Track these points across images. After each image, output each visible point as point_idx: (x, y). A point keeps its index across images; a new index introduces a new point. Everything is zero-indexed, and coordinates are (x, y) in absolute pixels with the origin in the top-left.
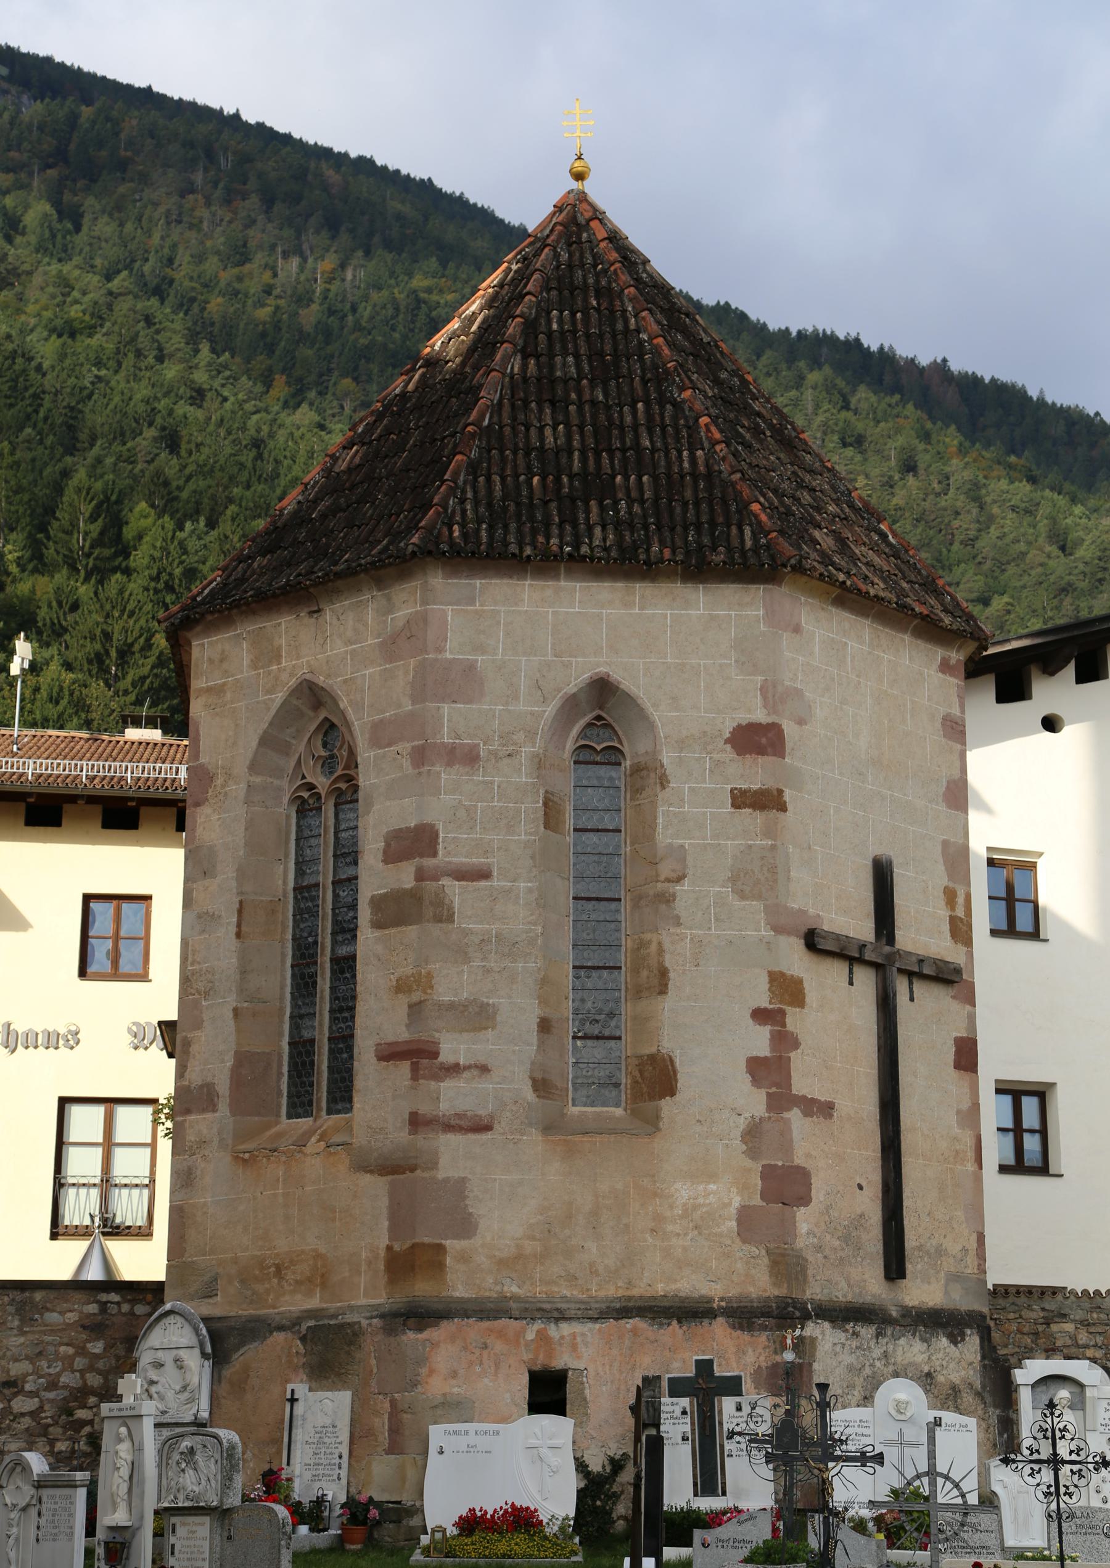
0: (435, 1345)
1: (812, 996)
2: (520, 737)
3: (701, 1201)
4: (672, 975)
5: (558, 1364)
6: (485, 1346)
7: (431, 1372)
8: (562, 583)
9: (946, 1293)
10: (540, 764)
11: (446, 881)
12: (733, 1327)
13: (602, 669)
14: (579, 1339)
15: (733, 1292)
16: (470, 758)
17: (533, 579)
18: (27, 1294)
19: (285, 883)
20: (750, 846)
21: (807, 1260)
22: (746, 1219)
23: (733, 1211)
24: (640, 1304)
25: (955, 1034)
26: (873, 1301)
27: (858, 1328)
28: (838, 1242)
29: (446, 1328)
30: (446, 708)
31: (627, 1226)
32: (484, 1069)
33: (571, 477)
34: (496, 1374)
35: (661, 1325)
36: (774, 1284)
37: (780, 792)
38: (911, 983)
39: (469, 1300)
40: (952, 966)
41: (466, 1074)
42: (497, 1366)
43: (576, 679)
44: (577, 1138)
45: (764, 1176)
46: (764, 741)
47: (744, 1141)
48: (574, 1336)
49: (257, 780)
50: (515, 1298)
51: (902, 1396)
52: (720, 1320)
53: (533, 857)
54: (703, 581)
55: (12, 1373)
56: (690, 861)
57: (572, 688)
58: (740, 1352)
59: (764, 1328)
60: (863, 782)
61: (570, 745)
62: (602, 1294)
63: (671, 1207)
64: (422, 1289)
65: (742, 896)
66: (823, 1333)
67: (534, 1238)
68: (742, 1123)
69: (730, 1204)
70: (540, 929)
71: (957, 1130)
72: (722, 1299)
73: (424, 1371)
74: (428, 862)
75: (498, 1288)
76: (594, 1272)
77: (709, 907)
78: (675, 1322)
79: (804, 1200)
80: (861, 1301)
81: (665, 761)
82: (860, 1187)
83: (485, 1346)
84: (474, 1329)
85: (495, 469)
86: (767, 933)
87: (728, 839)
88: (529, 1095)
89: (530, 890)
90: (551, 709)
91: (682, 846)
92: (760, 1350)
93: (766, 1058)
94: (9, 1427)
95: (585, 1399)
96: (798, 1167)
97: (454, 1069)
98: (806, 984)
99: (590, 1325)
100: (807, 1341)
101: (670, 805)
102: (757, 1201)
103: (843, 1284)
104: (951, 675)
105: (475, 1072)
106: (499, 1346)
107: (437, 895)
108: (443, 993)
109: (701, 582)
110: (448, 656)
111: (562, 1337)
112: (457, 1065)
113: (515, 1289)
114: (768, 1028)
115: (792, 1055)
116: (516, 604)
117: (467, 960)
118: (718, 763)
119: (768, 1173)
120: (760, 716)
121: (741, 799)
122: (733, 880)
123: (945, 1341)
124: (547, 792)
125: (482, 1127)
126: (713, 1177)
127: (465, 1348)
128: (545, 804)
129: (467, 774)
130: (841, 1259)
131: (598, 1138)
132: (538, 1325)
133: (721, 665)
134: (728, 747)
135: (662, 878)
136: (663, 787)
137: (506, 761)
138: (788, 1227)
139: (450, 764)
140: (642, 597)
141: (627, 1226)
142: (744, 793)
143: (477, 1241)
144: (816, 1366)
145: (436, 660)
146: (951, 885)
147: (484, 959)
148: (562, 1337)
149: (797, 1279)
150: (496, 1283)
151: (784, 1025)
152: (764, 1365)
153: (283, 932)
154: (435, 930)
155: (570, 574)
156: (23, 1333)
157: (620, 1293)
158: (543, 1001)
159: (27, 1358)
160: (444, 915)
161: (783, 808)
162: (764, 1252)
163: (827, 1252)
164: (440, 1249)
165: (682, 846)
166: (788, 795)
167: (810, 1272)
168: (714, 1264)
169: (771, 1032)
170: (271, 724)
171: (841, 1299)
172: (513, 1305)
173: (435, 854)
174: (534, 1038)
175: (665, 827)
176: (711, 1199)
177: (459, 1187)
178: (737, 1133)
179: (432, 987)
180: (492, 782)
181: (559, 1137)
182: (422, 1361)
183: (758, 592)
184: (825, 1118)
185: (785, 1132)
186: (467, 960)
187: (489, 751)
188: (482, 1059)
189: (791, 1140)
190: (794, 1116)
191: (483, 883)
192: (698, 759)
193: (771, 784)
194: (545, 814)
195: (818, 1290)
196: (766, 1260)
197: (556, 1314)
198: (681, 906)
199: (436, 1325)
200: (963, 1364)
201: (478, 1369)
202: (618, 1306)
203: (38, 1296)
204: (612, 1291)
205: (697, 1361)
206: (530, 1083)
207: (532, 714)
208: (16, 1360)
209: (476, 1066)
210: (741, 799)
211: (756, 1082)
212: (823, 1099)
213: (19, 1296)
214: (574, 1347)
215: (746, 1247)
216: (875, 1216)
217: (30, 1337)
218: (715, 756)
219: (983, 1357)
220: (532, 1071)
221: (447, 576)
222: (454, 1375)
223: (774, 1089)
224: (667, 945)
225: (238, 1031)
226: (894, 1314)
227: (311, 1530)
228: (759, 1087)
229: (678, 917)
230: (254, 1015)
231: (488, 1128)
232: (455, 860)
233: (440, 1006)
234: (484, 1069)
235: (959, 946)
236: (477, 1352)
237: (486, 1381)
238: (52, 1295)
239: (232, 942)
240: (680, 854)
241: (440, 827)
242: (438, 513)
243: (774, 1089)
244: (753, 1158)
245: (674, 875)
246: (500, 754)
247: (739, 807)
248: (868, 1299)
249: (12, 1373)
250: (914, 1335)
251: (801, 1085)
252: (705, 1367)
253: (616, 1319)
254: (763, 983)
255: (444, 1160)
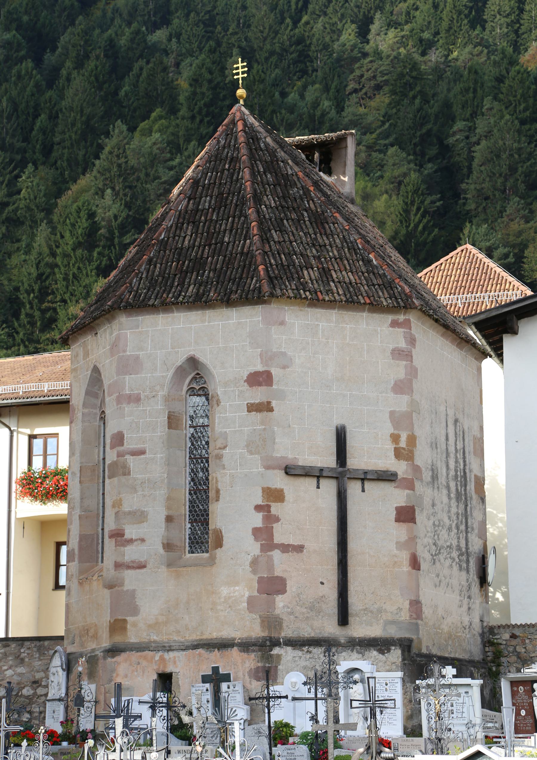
0: (119, 663)
1: (289, 495)
2: (158, 388)
3: (232, 595)
4: (221, 492)
5: (168, 670)
6: (139, 663)
7: (117, 675)
8: (175, 314)
9: (384, 629)
10: (167, 399)
11: (127, 457)
12: (241, 651)
13: (192, 353)
14: (177, 659)
15: (245, 635)
16: (136, 399)
17: (163, 314)
18: (42, 643)
19: (99, 456)
20: (255, 430)
21: (282, 619)
22: (251, 601)
23: (245, 598)
24: (205, 642)
25: (395, 505)
26: (330, 636)
27: (310, 649)
28: (305, 610)
29: (124, 655)
30: (127, 377)
31: (201, 607)
32: (143, 540)
33: (190, 261)
34: (143, 676)
35: (211, 651)
36: (262, 631)
37: (269, 403)
38: (363, 484)
39: (136, 643)
40: (390, 473)
41: (135, 543)
42: (143, 672)
43: (181, 359)
44: (181, 569)
45: (259, 582)
46: (261, 379)
47: (251, 567)
48: (175, 657)
49: (86, 411)
50: (155, 642)
51: (294, 680)
52: (235, 648)
53: (163, 443)
54: (235, 306)
55: (37, 677)
56: (229, 438)
57: (179, 363)
58: (243, 662)
59: (254, 651)
60: (330, 390)
61: (185, 388)
62: (191, 638)
63: (219, 598)
64: (118, 639)
65: (251, 453)
66: (286, 652)
67: (162, 615)
68: (250, 558)
69: (244, 595)
70: (166, 475)
71: (395, 552)
72: (239, 639)
73: (114, 675)
74: (121, 449)
75: (148, 638)
76: (187, 629)
77: (237, 459)
78: (216, 650)
79: (283, 591)
80: (321, 636)
81: (219, 393)
82: (322, 583)
83: (139, 663)
84: (134, 656)
85: (159, 261)
86: (261, 469)
87: (246, 427)
88: (161, 551)
89: (162, 458)
90: (170, 374)
91: (226, 432)
92: (251, 661)
93: (260, 528)
94: (36, 701)
95: (179, 685)
96: (277, 577)
97: (131, 541)
98: (285, 491)
99: (181, 652)
100: (275, 657)
101: (221, 413)
102: (256, 593)
103: (310, 630)
104: (398, 328)
105: (139, 542)
106: (144, 663)
107: (124, 463)
108: (126, 508)
109: (234, 307)
110: (128, 353)
111: (170, 658)
112: (132, 539)
113: (155, 638)
114: (262, 513)
115: (275, 525)
116: (156, 327)
117: (136, 491)
118: (241, 392)
119: (261, 581)
120: (260, 368)
121: (252, 408)
122: (247, 446)
123: (375, 653)
124: (169, 412)
125: (142, 566)
126: (237, 584)
127: (131, 665)
128: (169, 418)
129: (136, 407)
130: (307, 617)
131: (189, 569)
132: (160, 653)
133: (243, 345)
134: (246, 384)
135: (217, 448)
136: (218, 405)
137: (153, 399)
138: (272, 604)
139: (129, 403)
140: (209, 317)
141: (201, 607)
142: (252, 404)
143: (140, 617)
144: (280, 667)
145: (123, 356)
146: (396, 432)
147: (143, 491)
148: (170, 658)
149: (275, 628)
150: (148, 635)
151: (270, 512)
152: (253, 667)
153: (98, 479)
154: (123, 479)
155: (178, 310)
156: (41, 660)
157: (198, 638)
158: (168, 508)
159: (43, 671)
160: (126, 472)
161: (271, 410)
162: (258, 617)
163: (297, 615)
164: (125, 621)
165: (226, 432)
166: (274, 404)
167: (284, 625)
168: (237, 623)
169: (263, 516)
170: (88, 385)
171: (306, 635)
172: (153, 645)
173: (123, 445)
174: (163, 525)
175: (219, 424)
176: (237, 594)
177: (132, 594)
178: (248, 563)
179: (121, 505)
180: (146, 410)
181: (173, 569)
182: (113, 670)
183: (259, 308)
184: (298, 553)
185: (270, 559)
186: (136, 491)
187: (145, 396)
188: (142, 536)
189: (273, 565)
190: (276, 554)
191: (143, 456)
192: (233, 391)
193: (265, 400)
194: (169, 422)
195: (290, 632)
196: (259, 620)
197: (168, 648)
198: (225, 461)
199: (119, 655)
200: (388, 663)
201: (136, 673)
202: (196, 643)
203: (46, 643)
204: (194, 637)
205: (213, 667)
206: (161, 545)
207: (163, 376)
208: (38, 672)
209: (140, 539)
210: (252, 408)
211: (256, 539)
212: (296, 544)
213: (38, 643)
214: (175, 662)
215: (251, 615)
216: (333, 595)
217: (43, 661)
218: (240, 388)
219: (404, 660)
220: (162, 540)
221: (128, 317)
222: (126, 676)
223: (264, 542)
224: (219, 479)
225: (80, 525)
226: (342, 641)
227: (69, 744)
228: (257, 541)
229: (224, 465)
230: (86, 518)
231: (144, 567)
232: (131, 447)
233: (125, 513)
234: (143, 540)
235: (402, 461)
236: (135, 666)
237: (139, 678)
238: (52, 642)
239: (78, 485)
240: (225, 435)
241: (125, 433)
242: (127, 287)
243: (264, 542)
244: (254, 574)
245: (222, 446)
246: (150, 397)
247: (250, 412)
248: (326, 635)
249: (37, 677)
250: (352, 651)
251: (278, 538)
252: (216, 670)
253: (192, 649)
254: (260, 493)
255: (126, 582)
